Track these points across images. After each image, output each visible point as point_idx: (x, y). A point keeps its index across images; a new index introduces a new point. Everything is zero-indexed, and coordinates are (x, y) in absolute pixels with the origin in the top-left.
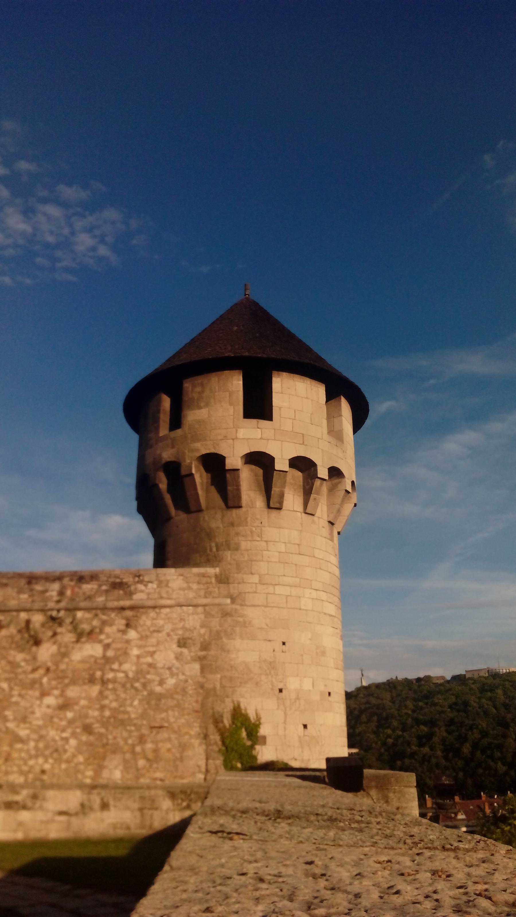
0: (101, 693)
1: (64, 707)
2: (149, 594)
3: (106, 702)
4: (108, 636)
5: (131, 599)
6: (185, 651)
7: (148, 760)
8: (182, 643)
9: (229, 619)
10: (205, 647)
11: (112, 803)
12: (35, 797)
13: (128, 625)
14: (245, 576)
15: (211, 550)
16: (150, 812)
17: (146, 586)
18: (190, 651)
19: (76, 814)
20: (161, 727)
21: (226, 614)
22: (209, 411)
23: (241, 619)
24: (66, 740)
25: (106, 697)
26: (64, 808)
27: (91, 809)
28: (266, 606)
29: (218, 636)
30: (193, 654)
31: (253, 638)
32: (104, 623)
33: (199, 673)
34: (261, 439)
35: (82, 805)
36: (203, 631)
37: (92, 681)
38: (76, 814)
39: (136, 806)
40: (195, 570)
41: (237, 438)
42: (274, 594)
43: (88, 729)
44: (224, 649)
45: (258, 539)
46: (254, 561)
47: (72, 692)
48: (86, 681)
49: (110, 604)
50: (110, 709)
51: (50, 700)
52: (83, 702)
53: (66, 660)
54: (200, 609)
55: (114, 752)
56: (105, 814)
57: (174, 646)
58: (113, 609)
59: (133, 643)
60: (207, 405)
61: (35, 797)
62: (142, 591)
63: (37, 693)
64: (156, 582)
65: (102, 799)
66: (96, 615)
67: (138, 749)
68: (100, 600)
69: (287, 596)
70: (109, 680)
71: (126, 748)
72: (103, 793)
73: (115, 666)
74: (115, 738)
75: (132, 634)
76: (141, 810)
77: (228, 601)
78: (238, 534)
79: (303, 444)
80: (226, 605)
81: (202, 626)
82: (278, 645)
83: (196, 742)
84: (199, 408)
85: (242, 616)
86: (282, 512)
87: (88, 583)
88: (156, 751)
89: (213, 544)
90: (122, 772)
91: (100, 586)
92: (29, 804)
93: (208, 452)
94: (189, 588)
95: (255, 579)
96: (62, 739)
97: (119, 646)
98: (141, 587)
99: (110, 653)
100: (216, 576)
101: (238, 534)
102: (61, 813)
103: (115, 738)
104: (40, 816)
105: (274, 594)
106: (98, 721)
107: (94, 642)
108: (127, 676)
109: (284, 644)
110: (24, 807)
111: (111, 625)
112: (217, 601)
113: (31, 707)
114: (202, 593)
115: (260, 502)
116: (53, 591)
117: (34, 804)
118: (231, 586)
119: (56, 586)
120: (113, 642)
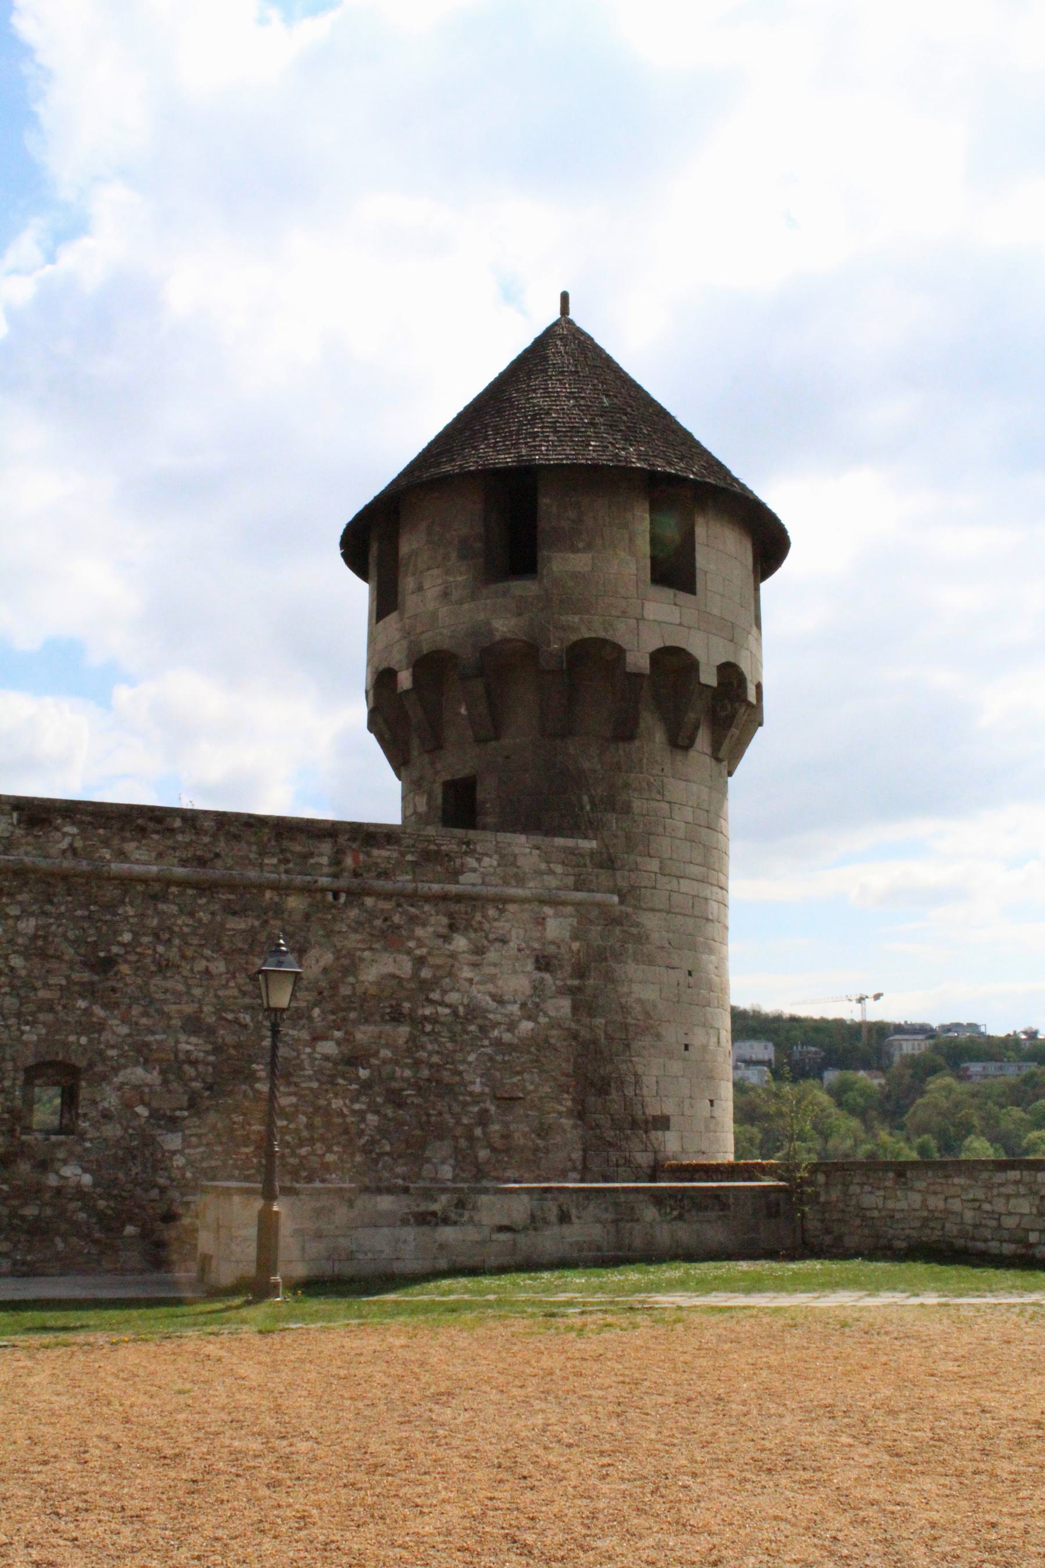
0: (412, 1039)
1: (353, 1059)
2: (484, 875)
3: (423, 1055)
4: (420, 944)
5: (457, 882)
6: (547, 976)
7: (494, 1150)
8: (544, 963)
9: (617, 930)
10: (580, 972)
11: (574, 1212)
12: (461, 1204)
13: (452, 927)
14: (639, 859)
15: (582, 808)
16: (629, 1225)
17: (479, 860)
18: (555, 979)
19: (525, 1229)
20: (511, 1099)
21: (613, 921)
22: (593, 558)
23: (634, 930)
24: (361, 1115)
25: (423, 1048)
26: (505, 1222)
27: (546, 1222)
28: (668, 912)
29: (601, 955)
30: (559, 983)
31: (652, 962)
32: (413, 920)
33: (570, 1015)
34: (680, 625)
35: (533, 1217)
36: (576, 946)
37: (396, 1017)
38: (525, 1229)
39: (610, 1216)
40: (560, 841)
41: (643, 618)
42: (678, 892)
43: (396, 1099)
44: (609, 977)
45: (658, 797)
46: (653, 834)
47: (363, 1034)
48: (387, 1017)
49: (424, 888)
50: (431, 1066)
51: (328, 1048)
52: (386, 1053)
53: (351, 979)
54: (569, 909)
55: (441, 1138)
56: (566, 1230)
57: (530, 966)
58: (428, 898)
59: (461, 957)
60: (589, 547)
61: (461, 1204)
62: (474, 870)
63: (305, 1035)
64: (496, 857)
65: (560, 1207)
66: (399, 905)
67: (478, 1132)
68: (404, 881)
69: (694, 897)
70: (425, 1018)
71: (459, 1130)
72: (561, 1198)
73: (435, 996)
74: (440, 1114)
75: (461, 943)
76: (615, 1221)
77: (616, 899)
78: (626, 786)
79: (732, 641)
80: (612, 905)
81: (575, 937)
82: (681, 975)
83: (566, 1122)
84: (575, 550)
85: (638, 925)
86: (692, 753)
87: (380, 847)
88: (506, 1137)
89: (585, 799)
90: (454, 1168)
91: (403, 855)
92: (453, 1216)
93: (593, 635)
94: (550, 872)
95: (654, 865)
96: (354, 1112)
97: (439, 961)
98: (471, 862)
99: (425, 973)
100: (592, 853)
101: (626, 786)
102: (501, 1229)
103: (440, 1114)
104: (472, 1234)
105: (678, 892)
106: (411, 1085)
107: (399, 951)
108: (455, 1013)
109: (690, 973)
110: (446, 1221)
111: (424, 925)
112: (599, 897)
113: (298, 1057)
114: (570, 881)
115: (660, 736)
116: (321, 855)
117: (461, 1215)
118: (618, 873)
119: (326, 847)
120: (429, 953)
